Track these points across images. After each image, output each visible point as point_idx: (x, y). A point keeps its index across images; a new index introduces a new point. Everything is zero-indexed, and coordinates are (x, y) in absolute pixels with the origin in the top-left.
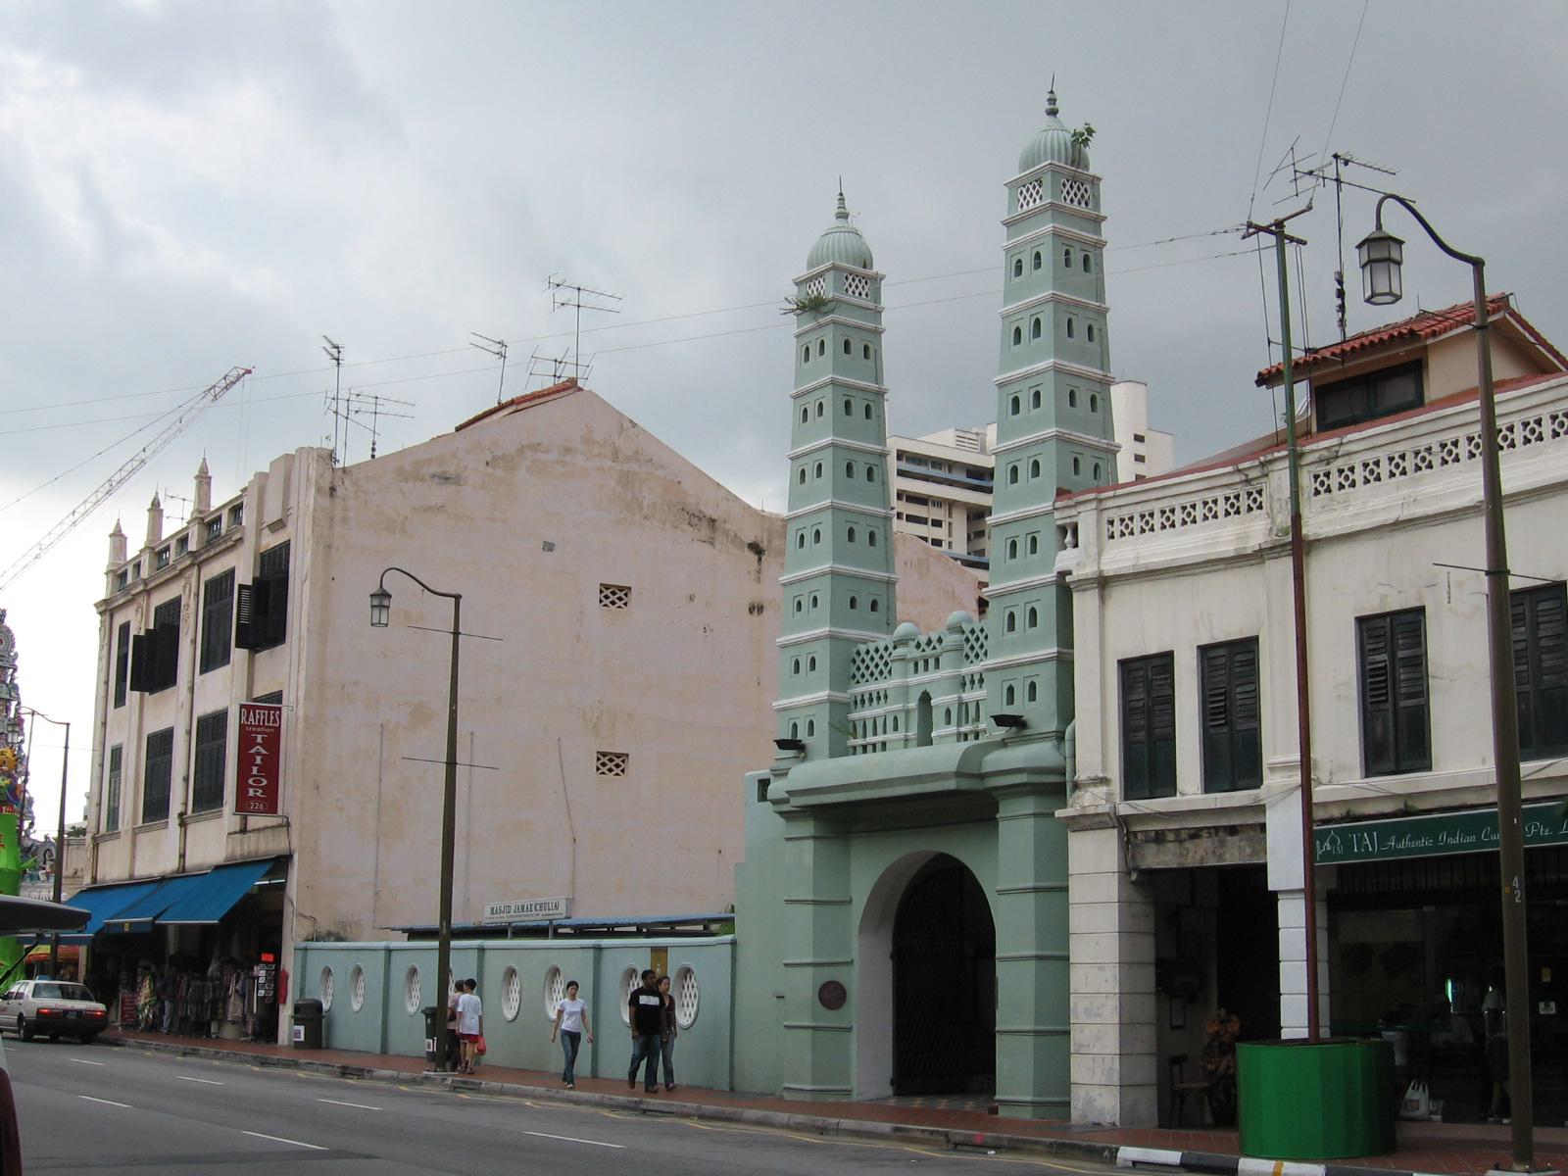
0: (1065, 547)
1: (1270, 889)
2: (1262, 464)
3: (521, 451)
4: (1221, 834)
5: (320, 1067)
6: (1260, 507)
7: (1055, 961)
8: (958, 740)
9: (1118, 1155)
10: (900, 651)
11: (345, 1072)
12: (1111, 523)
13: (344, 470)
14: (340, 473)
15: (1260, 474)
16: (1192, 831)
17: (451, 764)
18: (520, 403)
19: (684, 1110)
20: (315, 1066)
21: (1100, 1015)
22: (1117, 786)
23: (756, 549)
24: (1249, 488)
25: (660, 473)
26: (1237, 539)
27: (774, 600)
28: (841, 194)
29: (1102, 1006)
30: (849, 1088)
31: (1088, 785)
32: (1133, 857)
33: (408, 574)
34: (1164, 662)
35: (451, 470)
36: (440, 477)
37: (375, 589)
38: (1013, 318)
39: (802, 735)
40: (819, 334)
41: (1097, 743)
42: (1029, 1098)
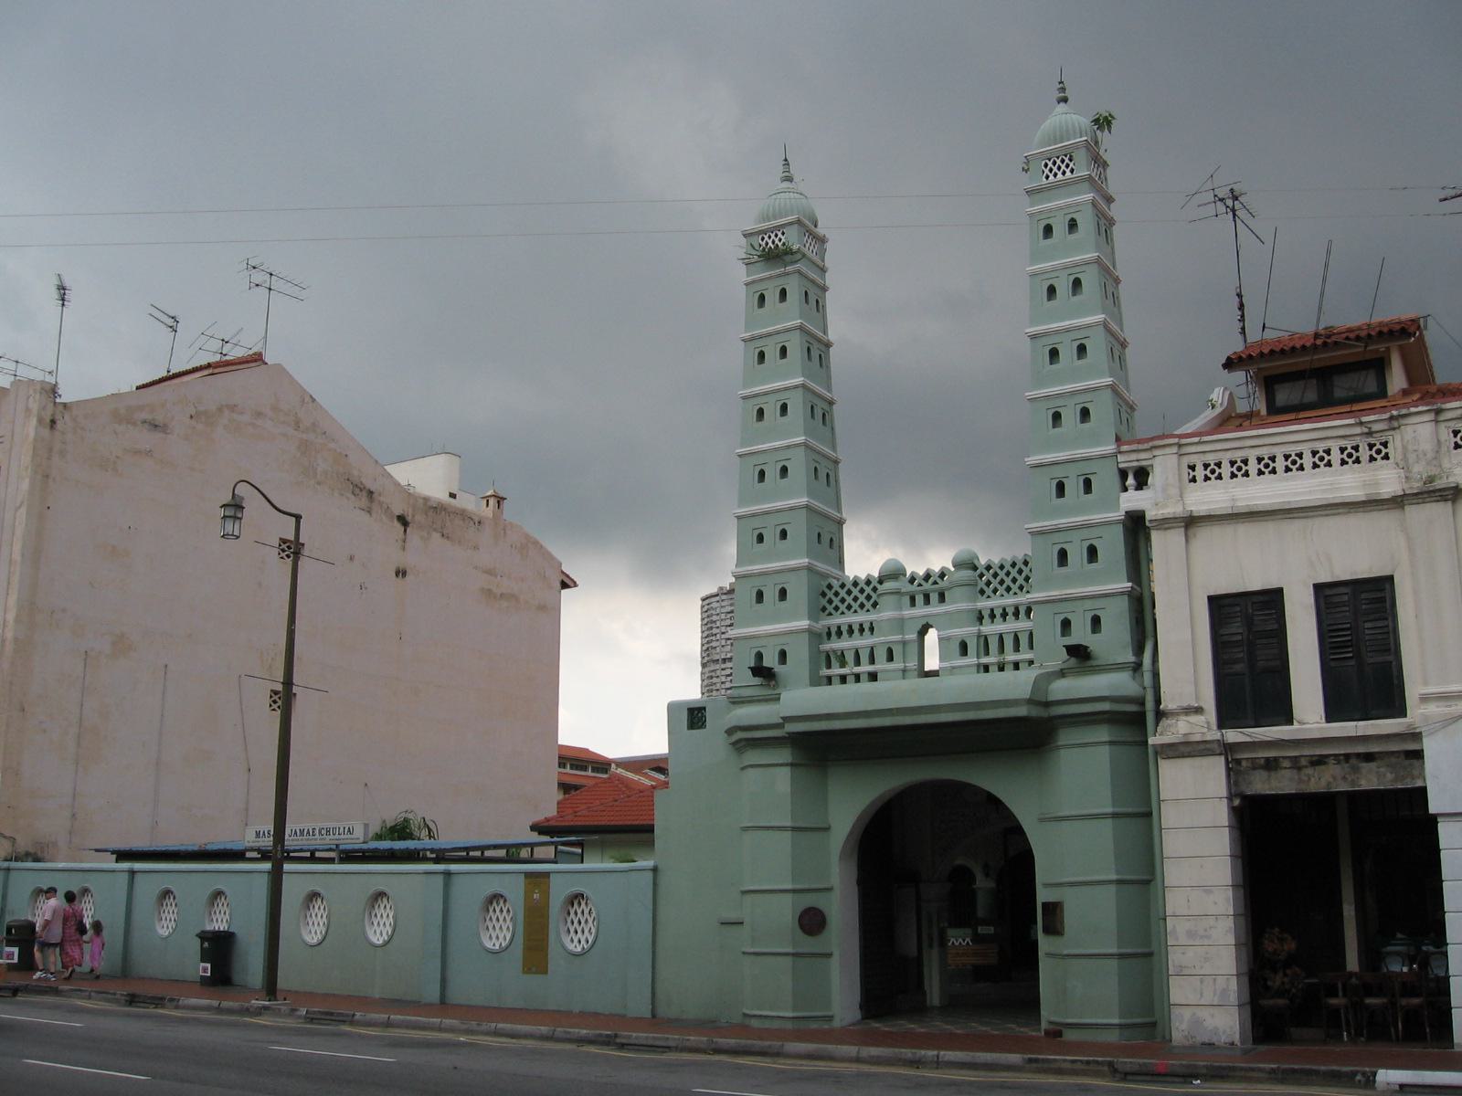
0: (1125, 489)
1: (1430, 812)
2: (1392, 418)
3: (220, 410)
4: (1353, 761)
5: (93, 994)
6: (1386, 457)
7: (1141, 878)
8: (978, 672)
9: (1377, 1078)
10: (888, 585)
11: (132, 1000)
12: (1193, 468)
13: (65, 405)
14: (61, 408)
15: (1386, 428)
16: (1314, 759)
17: (288, 684)
18: (215, 368)
19: (688, 1044)
20: (87, 994)
21: (1208, 937)
22: (1211, 713)
23: (403, 520)
24: (1343, 443)
25: (332, 445)
26: (1365, 485)
27: (415, 566)
28: (786, 160)
29: (1211, 928)
30: (830, 1013)
31: (1178, 714)
32: (1236, 783)
33: (258, 490)
34: (1272, 600)
35: (159, 418)
36: (150, 424)
37: (227, 498)
38: (1047, 276)
39: (770, 661)
40: (781, 282)
41: (1186, 668)
42: (1116, 1021)
